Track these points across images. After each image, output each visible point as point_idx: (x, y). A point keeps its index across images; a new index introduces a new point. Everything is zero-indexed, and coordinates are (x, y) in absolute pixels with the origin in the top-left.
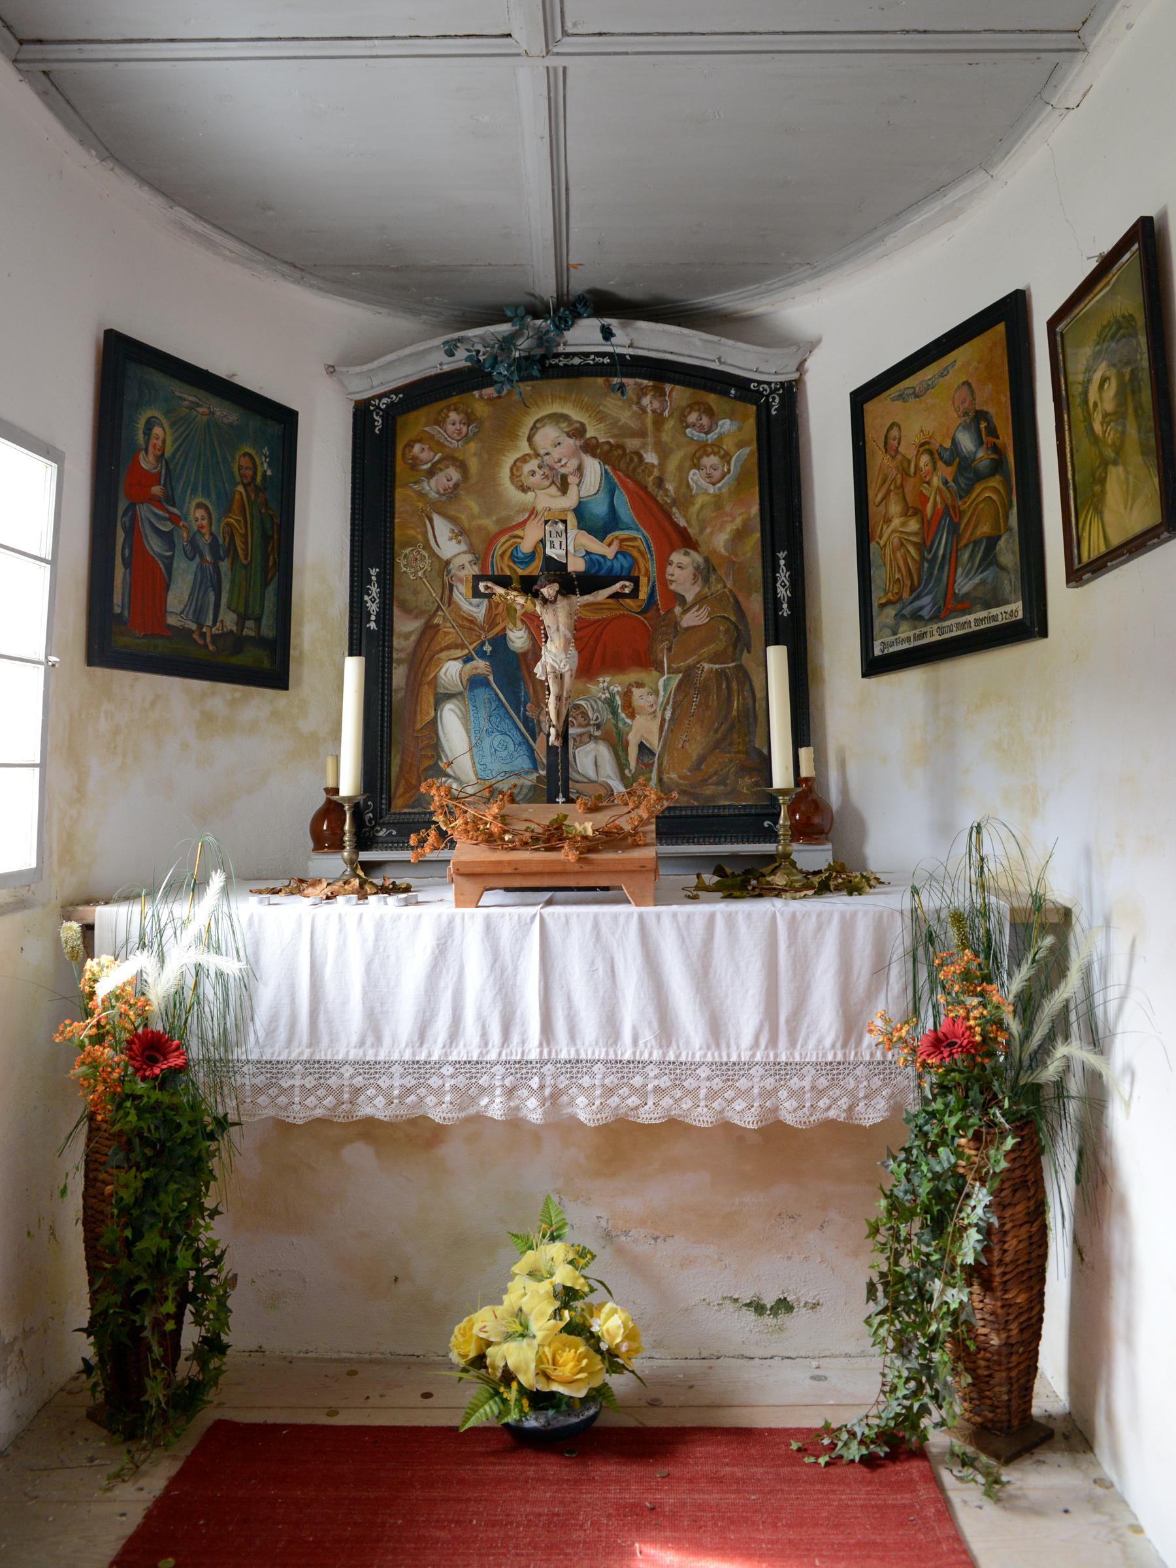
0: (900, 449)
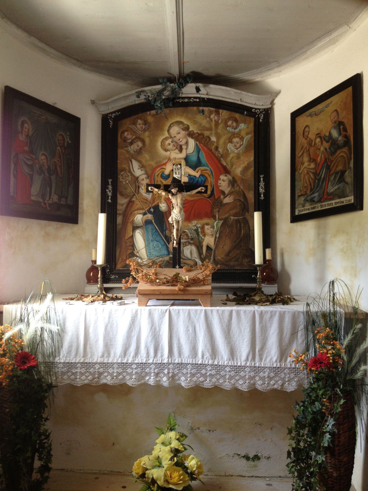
0: (309, 136)
